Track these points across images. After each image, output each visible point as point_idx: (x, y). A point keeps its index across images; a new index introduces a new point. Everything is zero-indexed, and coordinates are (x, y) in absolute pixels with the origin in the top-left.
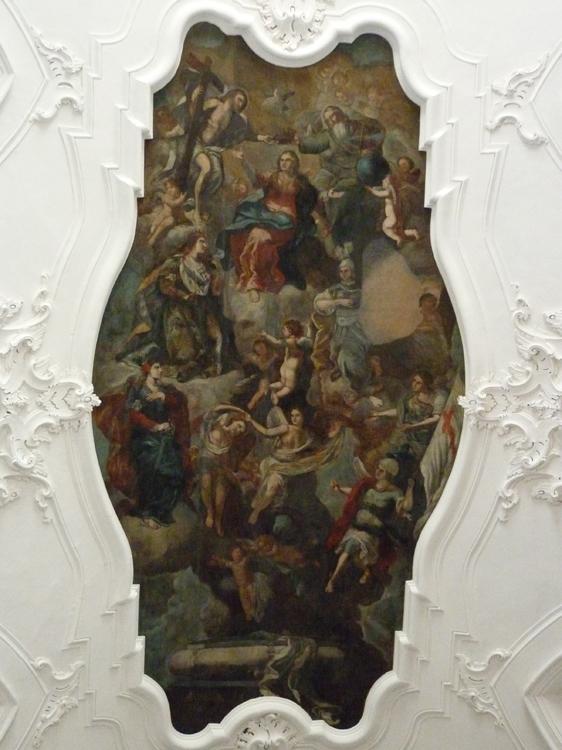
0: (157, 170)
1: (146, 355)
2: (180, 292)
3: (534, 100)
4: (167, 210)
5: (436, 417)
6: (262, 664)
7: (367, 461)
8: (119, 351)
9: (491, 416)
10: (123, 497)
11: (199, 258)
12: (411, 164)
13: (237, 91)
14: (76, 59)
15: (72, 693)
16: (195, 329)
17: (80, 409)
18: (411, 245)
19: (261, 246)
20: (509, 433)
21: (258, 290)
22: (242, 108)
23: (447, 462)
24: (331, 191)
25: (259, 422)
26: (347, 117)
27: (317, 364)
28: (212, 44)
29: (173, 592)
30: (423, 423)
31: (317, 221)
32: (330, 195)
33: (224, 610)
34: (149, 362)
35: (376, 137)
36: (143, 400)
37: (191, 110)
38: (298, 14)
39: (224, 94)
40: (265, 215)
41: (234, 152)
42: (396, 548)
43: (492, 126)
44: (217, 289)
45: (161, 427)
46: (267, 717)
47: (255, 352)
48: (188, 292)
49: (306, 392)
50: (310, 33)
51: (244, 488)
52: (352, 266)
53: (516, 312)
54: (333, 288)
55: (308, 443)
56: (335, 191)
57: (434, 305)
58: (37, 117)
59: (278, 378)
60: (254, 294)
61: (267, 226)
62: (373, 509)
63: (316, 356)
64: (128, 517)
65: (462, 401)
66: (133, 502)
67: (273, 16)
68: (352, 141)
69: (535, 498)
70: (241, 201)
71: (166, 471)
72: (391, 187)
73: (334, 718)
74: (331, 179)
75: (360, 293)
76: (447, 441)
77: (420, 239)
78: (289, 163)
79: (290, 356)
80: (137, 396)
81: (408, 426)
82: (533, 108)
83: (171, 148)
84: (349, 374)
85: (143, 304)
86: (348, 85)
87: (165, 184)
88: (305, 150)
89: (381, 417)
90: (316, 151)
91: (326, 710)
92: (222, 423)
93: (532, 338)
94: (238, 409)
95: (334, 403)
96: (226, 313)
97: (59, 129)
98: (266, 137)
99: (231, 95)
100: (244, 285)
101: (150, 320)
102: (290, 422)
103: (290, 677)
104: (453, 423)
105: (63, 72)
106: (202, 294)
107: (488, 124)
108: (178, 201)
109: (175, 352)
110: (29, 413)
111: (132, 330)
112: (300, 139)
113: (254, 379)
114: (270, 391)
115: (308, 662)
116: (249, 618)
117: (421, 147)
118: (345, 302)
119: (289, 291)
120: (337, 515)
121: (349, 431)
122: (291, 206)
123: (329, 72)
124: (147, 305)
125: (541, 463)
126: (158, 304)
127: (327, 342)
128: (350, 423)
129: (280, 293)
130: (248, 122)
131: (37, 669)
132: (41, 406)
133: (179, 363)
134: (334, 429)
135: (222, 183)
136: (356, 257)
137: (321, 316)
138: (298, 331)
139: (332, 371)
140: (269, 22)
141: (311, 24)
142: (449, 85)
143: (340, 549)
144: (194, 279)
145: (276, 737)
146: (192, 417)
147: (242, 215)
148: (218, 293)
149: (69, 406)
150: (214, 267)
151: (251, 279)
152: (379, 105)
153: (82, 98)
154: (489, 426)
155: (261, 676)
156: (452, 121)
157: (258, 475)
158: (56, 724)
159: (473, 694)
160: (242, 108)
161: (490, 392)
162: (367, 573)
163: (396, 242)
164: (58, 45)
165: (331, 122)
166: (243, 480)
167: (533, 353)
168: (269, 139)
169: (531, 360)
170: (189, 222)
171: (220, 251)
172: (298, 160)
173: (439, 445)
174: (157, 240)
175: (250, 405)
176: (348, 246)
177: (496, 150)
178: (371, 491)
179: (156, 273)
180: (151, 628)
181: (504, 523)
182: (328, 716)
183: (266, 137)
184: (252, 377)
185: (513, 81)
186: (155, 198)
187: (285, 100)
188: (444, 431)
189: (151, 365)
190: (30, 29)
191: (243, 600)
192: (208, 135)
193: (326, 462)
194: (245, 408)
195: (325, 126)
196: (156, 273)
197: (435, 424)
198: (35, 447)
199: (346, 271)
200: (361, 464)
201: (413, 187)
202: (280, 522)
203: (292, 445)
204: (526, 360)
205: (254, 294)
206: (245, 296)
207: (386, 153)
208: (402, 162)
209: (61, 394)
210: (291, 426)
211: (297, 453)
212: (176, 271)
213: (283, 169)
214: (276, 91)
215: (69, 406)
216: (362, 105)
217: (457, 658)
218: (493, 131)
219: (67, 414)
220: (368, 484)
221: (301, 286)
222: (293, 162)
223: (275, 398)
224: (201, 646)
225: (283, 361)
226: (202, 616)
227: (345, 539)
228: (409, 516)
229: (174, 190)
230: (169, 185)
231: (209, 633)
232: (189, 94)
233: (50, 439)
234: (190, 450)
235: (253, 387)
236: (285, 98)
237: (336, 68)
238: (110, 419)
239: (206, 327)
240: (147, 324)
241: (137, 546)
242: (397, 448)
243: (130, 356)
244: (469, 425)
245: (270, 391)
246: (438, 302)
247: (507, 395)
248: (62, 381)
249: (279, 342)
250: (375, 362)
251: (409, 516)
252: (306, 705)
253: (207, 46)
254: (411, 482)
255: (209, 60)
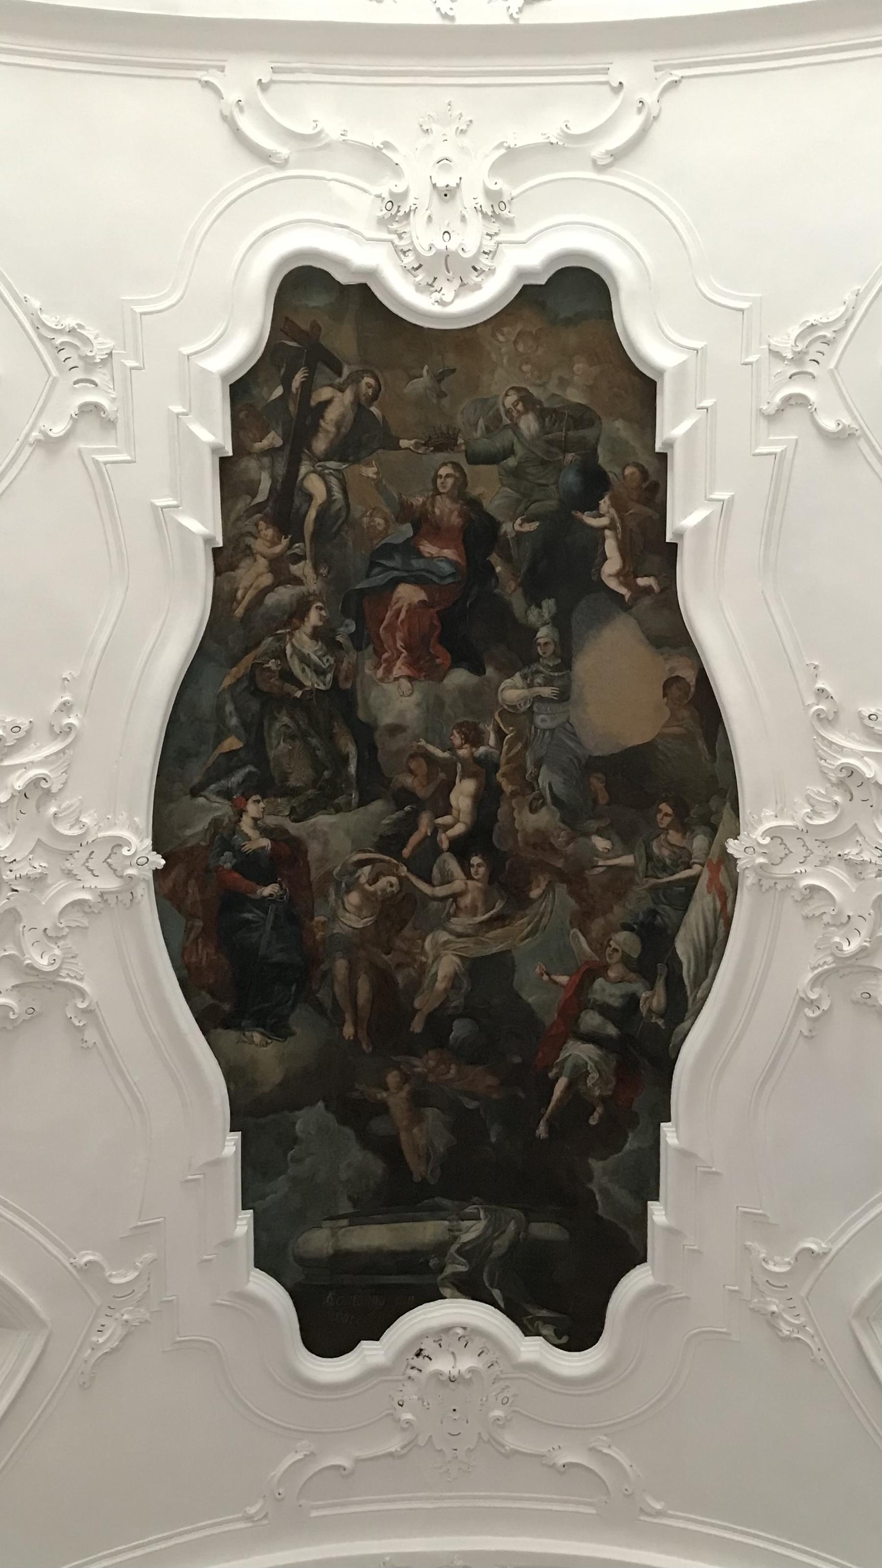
0: (241, 505)
1: (239, 785)
2: (288, 687)
3: (836, 367)
4: (262, 562)
5: (697, 868)
6: (440, 1249)
7: (594, 934)
8: (196, 780)
9: (780, 871)
10: (209, 1000)
11: (316, 635)
12: (644, 472)
13: (365, 372)
14: (100, 340)
15: (139, 1303)
16: (314, 741)
17: (130, 877)
18: (647, 601)
19: (412, 610)
20: (811, 898)
21: (410, 679)
22: (375, 397)
23: (716, 936)
24: (519, 521)
25: (420, 877)
26: (540, 403)
27: (508, 788)
28: (319, 300)
29: (296, 1140)
30: (677, 876)
31: (498, 569)
32: (517, 528)
33: (377, 1167)
34: (243, 795)
35: (588, 433)
36: (237, 852)
37: (293, 408)
38: (453, 246)
39: (341, 380)
40: (416, 563)
41: (364, 468)
42: (643, 1072)
43: (771, 410)
44: (346, 679)
45: (267, 891)
46: (451, 1332)
47: (411, 772)
48: (301, 685)
49: (492, 831)
50: (476, 273)
51: (400, 979)
52: (556, 636)
53: (816, 707)
54: (526, 671)
55: (499, 905)
56: (525, 521)
57: (687, 694)
58: (41, 437)
59: (447, 809)
60: (405, 684)
61: (418, 580)
62: (604, 1010)
63: (504, 775)
64: (220, 1030)
65: (733, 847)
66: (227, 1007)
67: (415, 249)
68: (549, 442)
69: (856, 1003)
70: (378, 543)
71: (278, 957)
72: (612, 511)
73: (559, 1335)
74: (518, 502)
75: (569, 678)
76: (715, 905)
77: (662, 591)
78: (450, 481)
79: (463, 777)
80: (227, 845)
81: (653, 881)
82: (835, 381)
83: (262, 468)
84: (556, 800)
85: (229, 708)
86: (540, 352)
87: (257, 525)
88: (474, 459)
89: (610, 867)
90: (492, 459)
91: (546, 1321)
92: (363, 880)
93: (841, 749)
94: (387, 858)
95: (535, 846)
96: (361, 715)
97: (80, 451)
98: (413, 442)
99: (354, 379)
100: (388, 671)
101: (242, 732)
102: (469, 876)
103: (486, 1269)
104: (723, 877)
105: (80, 364)
106: (322, 687)
107: (764, 407)
108: (278, 549)
109: (285, 777)
110: (50, 886)
111: (215, 748)
112: (466, 443)
113: (408, 813)
114: (436, 830)
115: (514, 1245)
116: (417, 1178)
117: (658, 448)
118: (547, 691)
119: (459, 677)
120: (550, 1018)
121: (561, 889)
122: (456, 548)
123: (509, 332)
124: (236, 709)
125: (863, 949)
126: (255, 706)
127: (520, 755)
128: (561, 876)
129: (445, 681)
130: (384, 417)
131: (80, 1269)
132: (70, 874)
133: (293, 792)
134: (538, 886)
135: (347, 518)
136: (561, 622)
137: (510, 713)
138: (475, 738)
139: (531, 797)
140: (410, 260)
141: (476, 257)
142: (698, 345)
143: (555, 1071)
144: (309, 666)
145: (466, 1363)
146: (314, 875)
147: (382, 565)
148: (348, 686)
149: (115, 871)
150: (340, 646)
151: (399, 663)
152: (591, 382)
153: (113, 400)
154: (779, 887)
155: (442, 1269)
156: (707, 403)
157: (424, 959)
158: (113, 1350)
159: (774, 1308)
160: (375, 397)
161: (775, 834)
162: (600, 1109)
163: (623, 596)
164: (70, 322)
165: (515, 414)
166: (399, 966)
167: (843, 775)
168: (417, 445)
169: (841, 784)
170: (297, 581)
171: (348, 621)
172: (464, 474)
173: (703, 911)
174: (247, 610)
175: (406, 852)
176: (549, 606)
177: (778, 449)
178: (599, 982)
179: (248, 660)
180: (263, 1197)
181: (810, 1038)
182: (548, 1331)
183: (413, 442)
184: (407, 808)
185: (800, 337)
186: (242, 546)
187: (439, 381)
188: (709, 887)
189: (247, 800)
190: (22, 302)
191: (405, 1147)
192: (320, 445)
193: (527, 937)
194: (398, 855)
195: (506, 421)
196: (248, 660)
197: (695, 879)
198: (63, 937)
199: (546, 644)
200: (582, 939)
201: (649, 511)
202: (460, 1029)
203: (473, 911)
204: (833, 785)
205: (405, 683)
206: (391, 688)
207: (603, 459)
208: (629, 471)
209: (101, 854)
210: (470, 883)
211: (481, 923)
212: (280, 655)
213: (441, 490)
214: (426, 367)
215: (115, 871)
216: (563, 383)
217: (747, 1248)
218: (773, 418)
219: (110, 884)
220: (600, 970)
221: (478, 669)
222: (456, 479)
223: (444, 840)
224: (345, 1222)
225: (454, 784)
226: (344, 1176)
227: (562, 1056)
228: (660, 1022)
229: (270, 532)
230: (262, 524)
231: (354, 1202)
232: (286, 383)
233: (85, 922)
234: (314, 923)
235: (410, 824)
236: (439, 378)
237: (519, 327)
238: (186, 883)
239: (331, 737)
240: (239, 738)
241: (231, 1073)
242: (637, 916)
243: (212, 787)
244: (747, 882)
245: (436, 830)
246: (693, 689)
247: (806, 838)
248: (100, 835)
249: (447, 755)
250: (597, 783)
251: (660, 1022)
252: (513, 1313)
253: (312, 304)
254: (662, 969)
255: (315, 326)
